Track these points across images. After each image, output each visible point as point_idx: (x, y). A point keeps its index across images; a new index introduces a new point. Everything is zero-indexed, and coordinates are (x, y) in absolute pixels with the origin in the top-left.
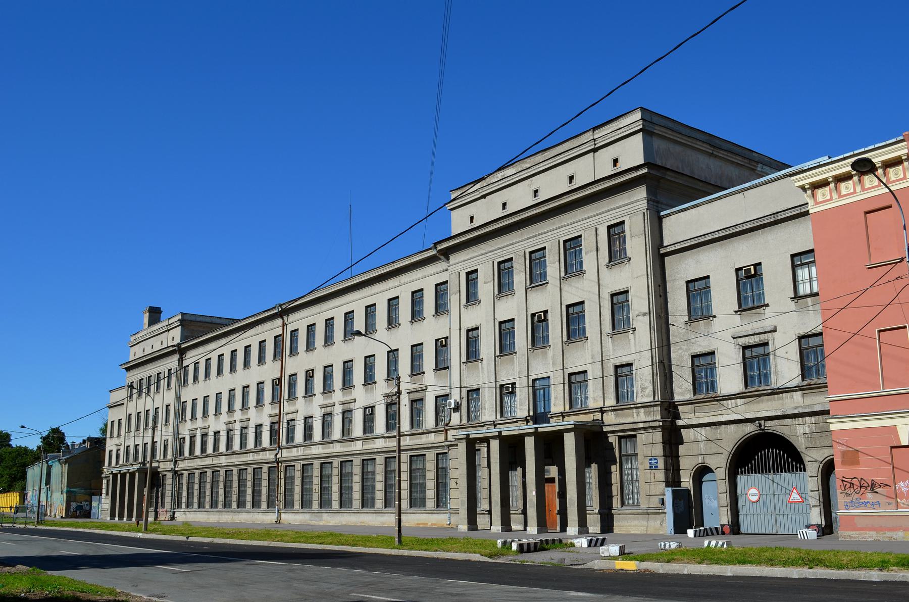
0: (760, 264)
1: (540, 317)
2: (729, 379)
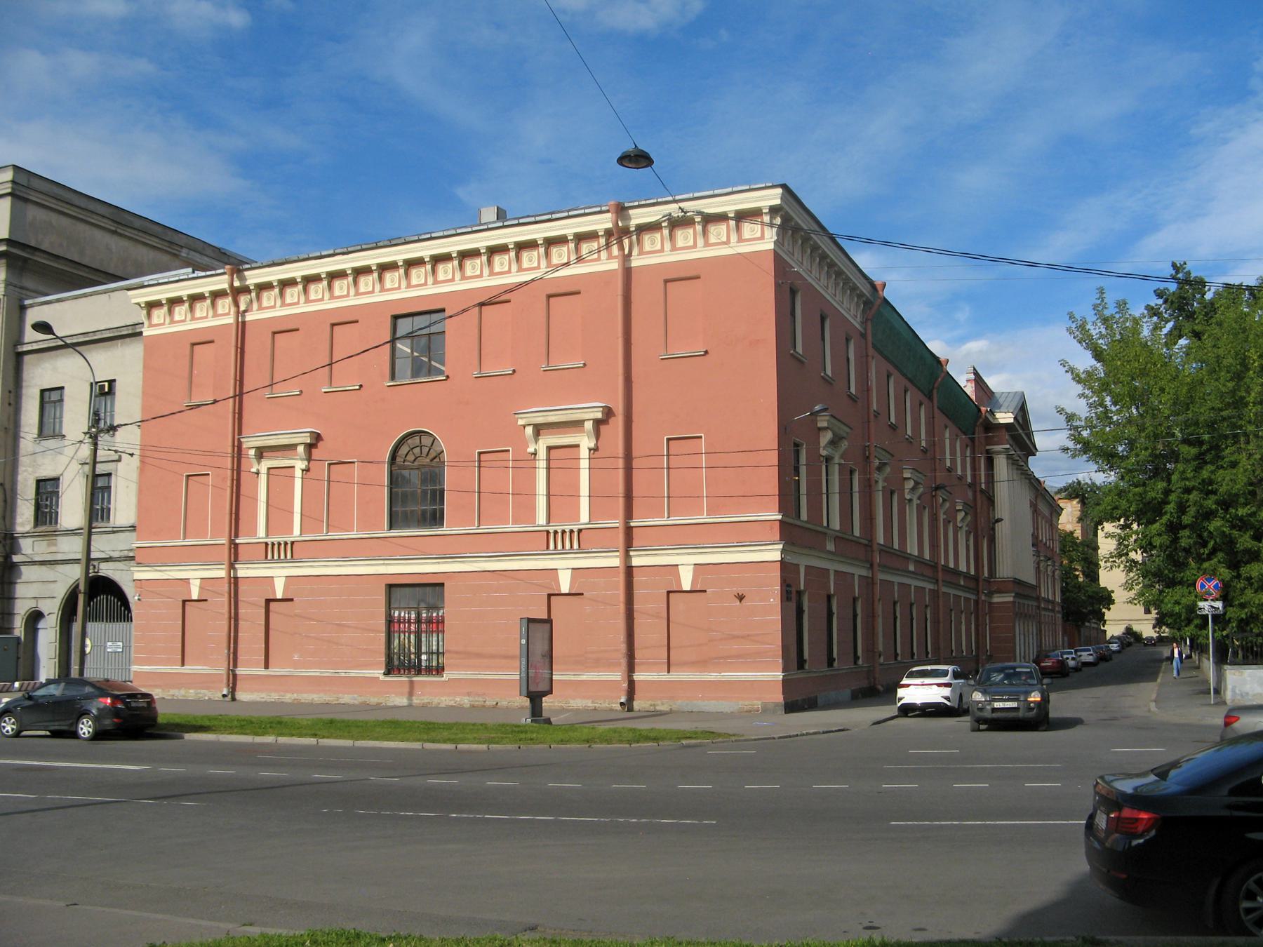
0: (114, 380)
1: (102, 387)
2: (72, 510)
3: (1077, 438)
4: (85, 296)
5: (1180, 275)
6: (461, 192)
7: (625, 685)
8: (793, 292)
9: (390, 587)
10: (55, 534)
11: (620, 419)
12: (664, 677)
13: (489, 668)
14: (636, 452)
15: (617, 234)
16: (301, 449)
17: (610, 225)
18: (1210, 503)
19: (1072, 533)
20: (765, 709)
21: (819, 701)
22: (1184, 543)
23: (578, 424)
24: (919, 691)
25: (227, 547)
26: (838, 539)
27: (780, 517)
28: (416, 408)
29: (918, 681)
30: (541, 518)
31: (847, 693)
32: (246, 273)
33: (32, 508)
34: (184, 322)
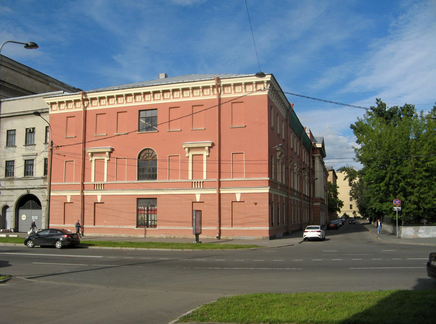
1: (30, 130)
3: (358, 156)
4: (23, 99)
5: (379, 103)
6: (115, 57)
7: (218, 231)
8: (271, 107)
9: (138, 199)
10: (13, 179)
11: (217, 147)
12: (231, 228)
13: (172, 225)
14: (222, 159)
15: (218, 86)
16: (107, 153)
17: (214, 84)
18: (399, 177)
19: (330, 182)
20: (263, 239)
21: (277, 237)
22: (390, 189)
23: (203, 148)
24: (310, 233)
25: (81, 185)
26: (281, 185)
27: (269, 179)
28: (147, 140)
29: (311, 230)
30: (190, 178)
31: (281, 234)
32: (87, 94)
33: (4, 171)
34: (64, 110)
